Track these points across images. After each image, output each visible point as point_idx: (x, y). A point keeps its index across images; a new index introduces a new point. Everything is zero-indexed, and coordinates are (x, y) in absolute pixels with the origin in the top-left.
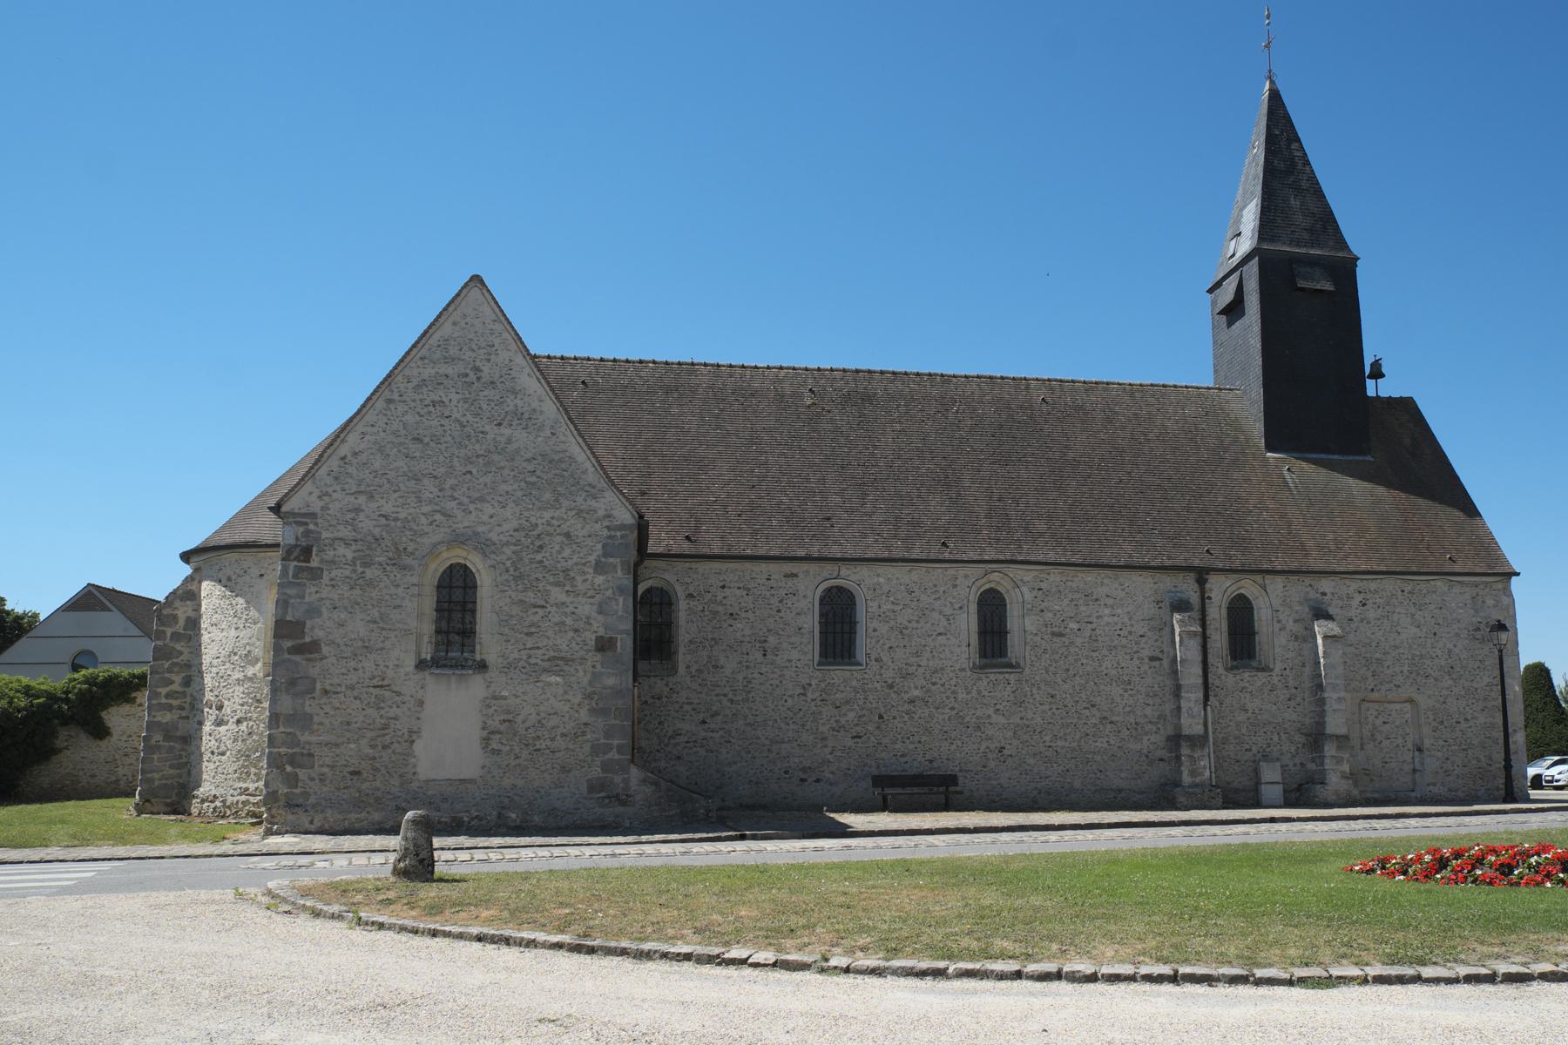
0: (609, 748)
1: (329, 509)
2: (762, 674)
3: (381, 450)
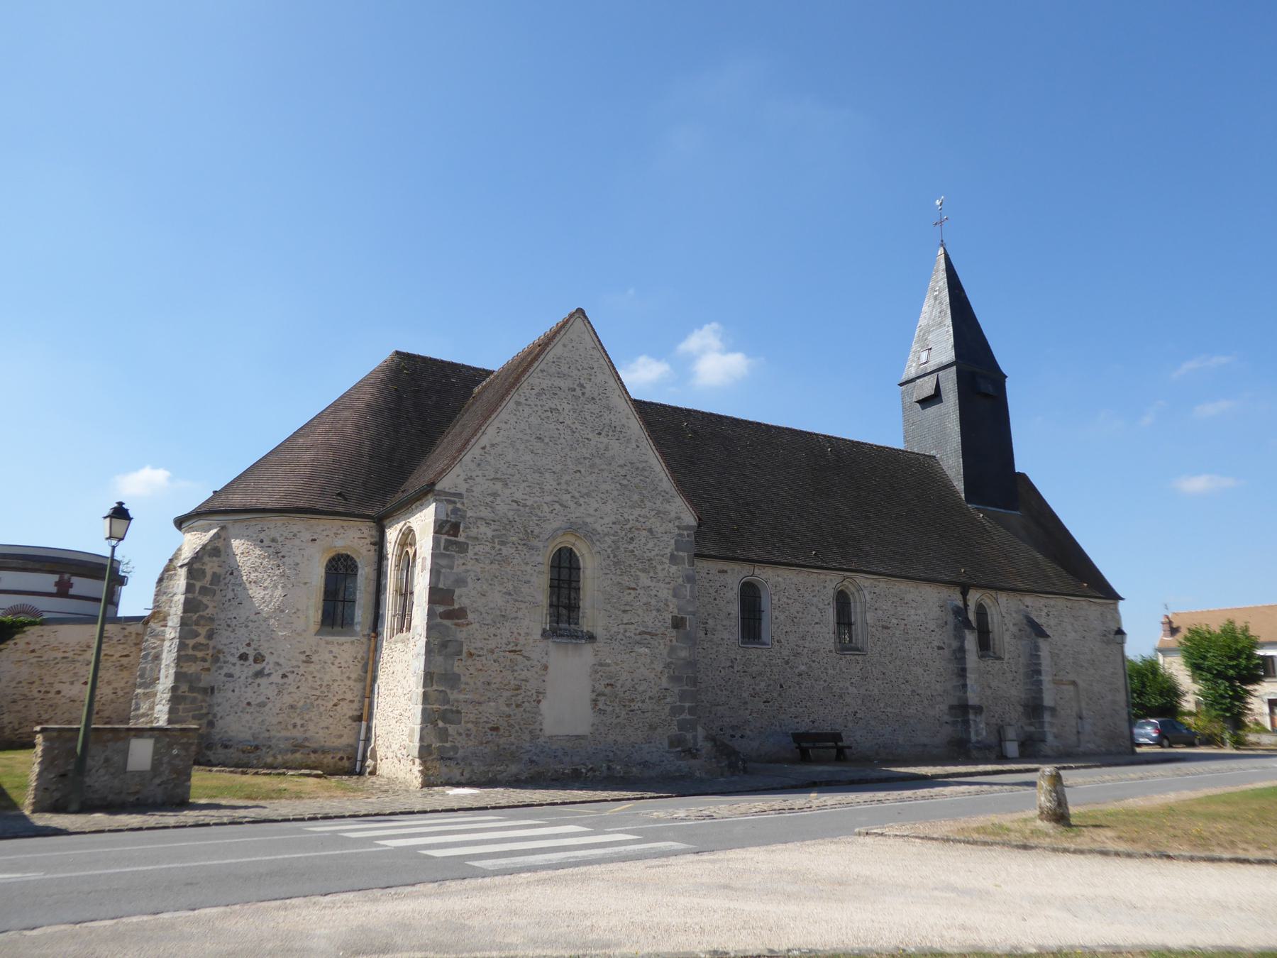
0: (682, 709)
1: (473, 492)
2: (704, 649)
3: (512, 444)
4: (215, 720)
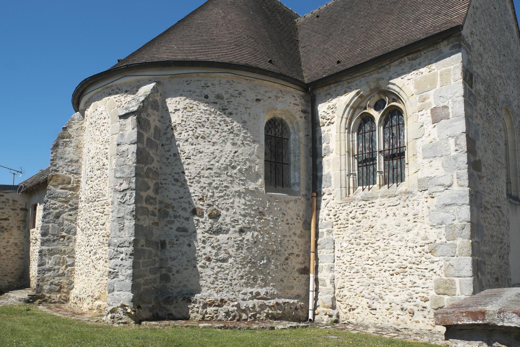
4: (170, 274)
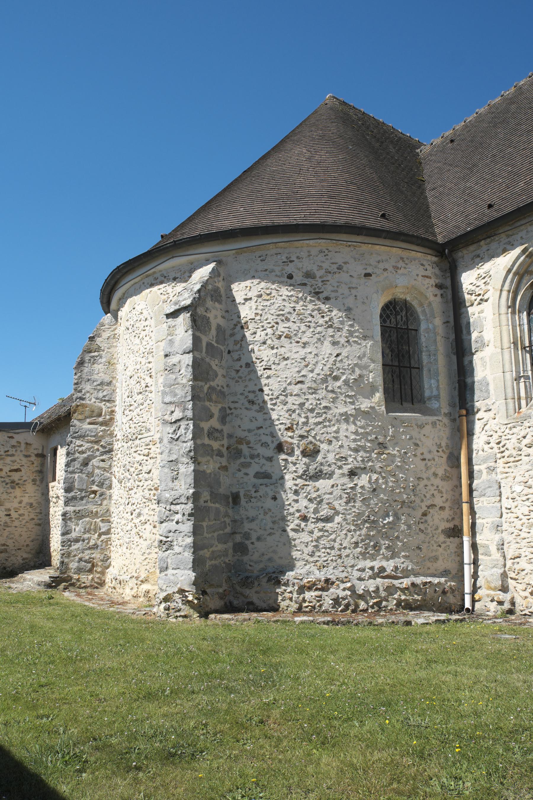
4: (248, 542)
